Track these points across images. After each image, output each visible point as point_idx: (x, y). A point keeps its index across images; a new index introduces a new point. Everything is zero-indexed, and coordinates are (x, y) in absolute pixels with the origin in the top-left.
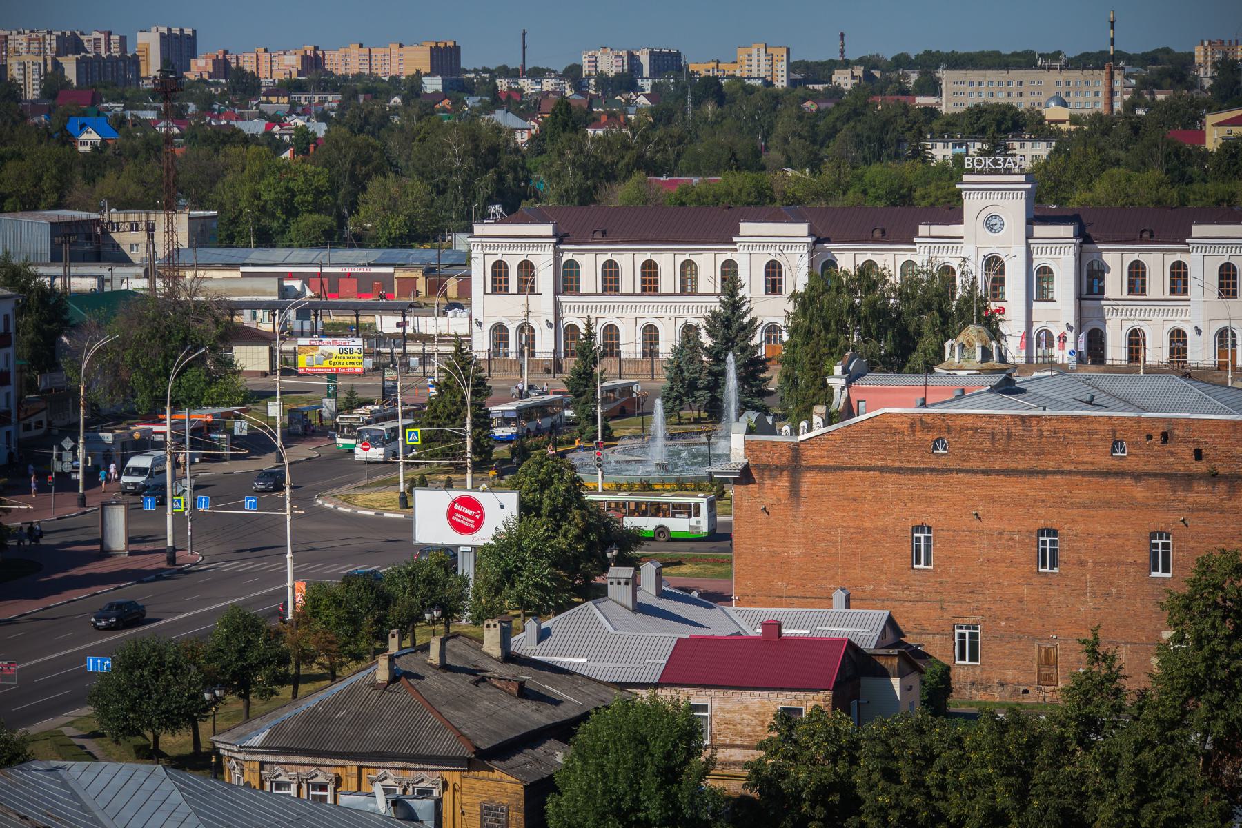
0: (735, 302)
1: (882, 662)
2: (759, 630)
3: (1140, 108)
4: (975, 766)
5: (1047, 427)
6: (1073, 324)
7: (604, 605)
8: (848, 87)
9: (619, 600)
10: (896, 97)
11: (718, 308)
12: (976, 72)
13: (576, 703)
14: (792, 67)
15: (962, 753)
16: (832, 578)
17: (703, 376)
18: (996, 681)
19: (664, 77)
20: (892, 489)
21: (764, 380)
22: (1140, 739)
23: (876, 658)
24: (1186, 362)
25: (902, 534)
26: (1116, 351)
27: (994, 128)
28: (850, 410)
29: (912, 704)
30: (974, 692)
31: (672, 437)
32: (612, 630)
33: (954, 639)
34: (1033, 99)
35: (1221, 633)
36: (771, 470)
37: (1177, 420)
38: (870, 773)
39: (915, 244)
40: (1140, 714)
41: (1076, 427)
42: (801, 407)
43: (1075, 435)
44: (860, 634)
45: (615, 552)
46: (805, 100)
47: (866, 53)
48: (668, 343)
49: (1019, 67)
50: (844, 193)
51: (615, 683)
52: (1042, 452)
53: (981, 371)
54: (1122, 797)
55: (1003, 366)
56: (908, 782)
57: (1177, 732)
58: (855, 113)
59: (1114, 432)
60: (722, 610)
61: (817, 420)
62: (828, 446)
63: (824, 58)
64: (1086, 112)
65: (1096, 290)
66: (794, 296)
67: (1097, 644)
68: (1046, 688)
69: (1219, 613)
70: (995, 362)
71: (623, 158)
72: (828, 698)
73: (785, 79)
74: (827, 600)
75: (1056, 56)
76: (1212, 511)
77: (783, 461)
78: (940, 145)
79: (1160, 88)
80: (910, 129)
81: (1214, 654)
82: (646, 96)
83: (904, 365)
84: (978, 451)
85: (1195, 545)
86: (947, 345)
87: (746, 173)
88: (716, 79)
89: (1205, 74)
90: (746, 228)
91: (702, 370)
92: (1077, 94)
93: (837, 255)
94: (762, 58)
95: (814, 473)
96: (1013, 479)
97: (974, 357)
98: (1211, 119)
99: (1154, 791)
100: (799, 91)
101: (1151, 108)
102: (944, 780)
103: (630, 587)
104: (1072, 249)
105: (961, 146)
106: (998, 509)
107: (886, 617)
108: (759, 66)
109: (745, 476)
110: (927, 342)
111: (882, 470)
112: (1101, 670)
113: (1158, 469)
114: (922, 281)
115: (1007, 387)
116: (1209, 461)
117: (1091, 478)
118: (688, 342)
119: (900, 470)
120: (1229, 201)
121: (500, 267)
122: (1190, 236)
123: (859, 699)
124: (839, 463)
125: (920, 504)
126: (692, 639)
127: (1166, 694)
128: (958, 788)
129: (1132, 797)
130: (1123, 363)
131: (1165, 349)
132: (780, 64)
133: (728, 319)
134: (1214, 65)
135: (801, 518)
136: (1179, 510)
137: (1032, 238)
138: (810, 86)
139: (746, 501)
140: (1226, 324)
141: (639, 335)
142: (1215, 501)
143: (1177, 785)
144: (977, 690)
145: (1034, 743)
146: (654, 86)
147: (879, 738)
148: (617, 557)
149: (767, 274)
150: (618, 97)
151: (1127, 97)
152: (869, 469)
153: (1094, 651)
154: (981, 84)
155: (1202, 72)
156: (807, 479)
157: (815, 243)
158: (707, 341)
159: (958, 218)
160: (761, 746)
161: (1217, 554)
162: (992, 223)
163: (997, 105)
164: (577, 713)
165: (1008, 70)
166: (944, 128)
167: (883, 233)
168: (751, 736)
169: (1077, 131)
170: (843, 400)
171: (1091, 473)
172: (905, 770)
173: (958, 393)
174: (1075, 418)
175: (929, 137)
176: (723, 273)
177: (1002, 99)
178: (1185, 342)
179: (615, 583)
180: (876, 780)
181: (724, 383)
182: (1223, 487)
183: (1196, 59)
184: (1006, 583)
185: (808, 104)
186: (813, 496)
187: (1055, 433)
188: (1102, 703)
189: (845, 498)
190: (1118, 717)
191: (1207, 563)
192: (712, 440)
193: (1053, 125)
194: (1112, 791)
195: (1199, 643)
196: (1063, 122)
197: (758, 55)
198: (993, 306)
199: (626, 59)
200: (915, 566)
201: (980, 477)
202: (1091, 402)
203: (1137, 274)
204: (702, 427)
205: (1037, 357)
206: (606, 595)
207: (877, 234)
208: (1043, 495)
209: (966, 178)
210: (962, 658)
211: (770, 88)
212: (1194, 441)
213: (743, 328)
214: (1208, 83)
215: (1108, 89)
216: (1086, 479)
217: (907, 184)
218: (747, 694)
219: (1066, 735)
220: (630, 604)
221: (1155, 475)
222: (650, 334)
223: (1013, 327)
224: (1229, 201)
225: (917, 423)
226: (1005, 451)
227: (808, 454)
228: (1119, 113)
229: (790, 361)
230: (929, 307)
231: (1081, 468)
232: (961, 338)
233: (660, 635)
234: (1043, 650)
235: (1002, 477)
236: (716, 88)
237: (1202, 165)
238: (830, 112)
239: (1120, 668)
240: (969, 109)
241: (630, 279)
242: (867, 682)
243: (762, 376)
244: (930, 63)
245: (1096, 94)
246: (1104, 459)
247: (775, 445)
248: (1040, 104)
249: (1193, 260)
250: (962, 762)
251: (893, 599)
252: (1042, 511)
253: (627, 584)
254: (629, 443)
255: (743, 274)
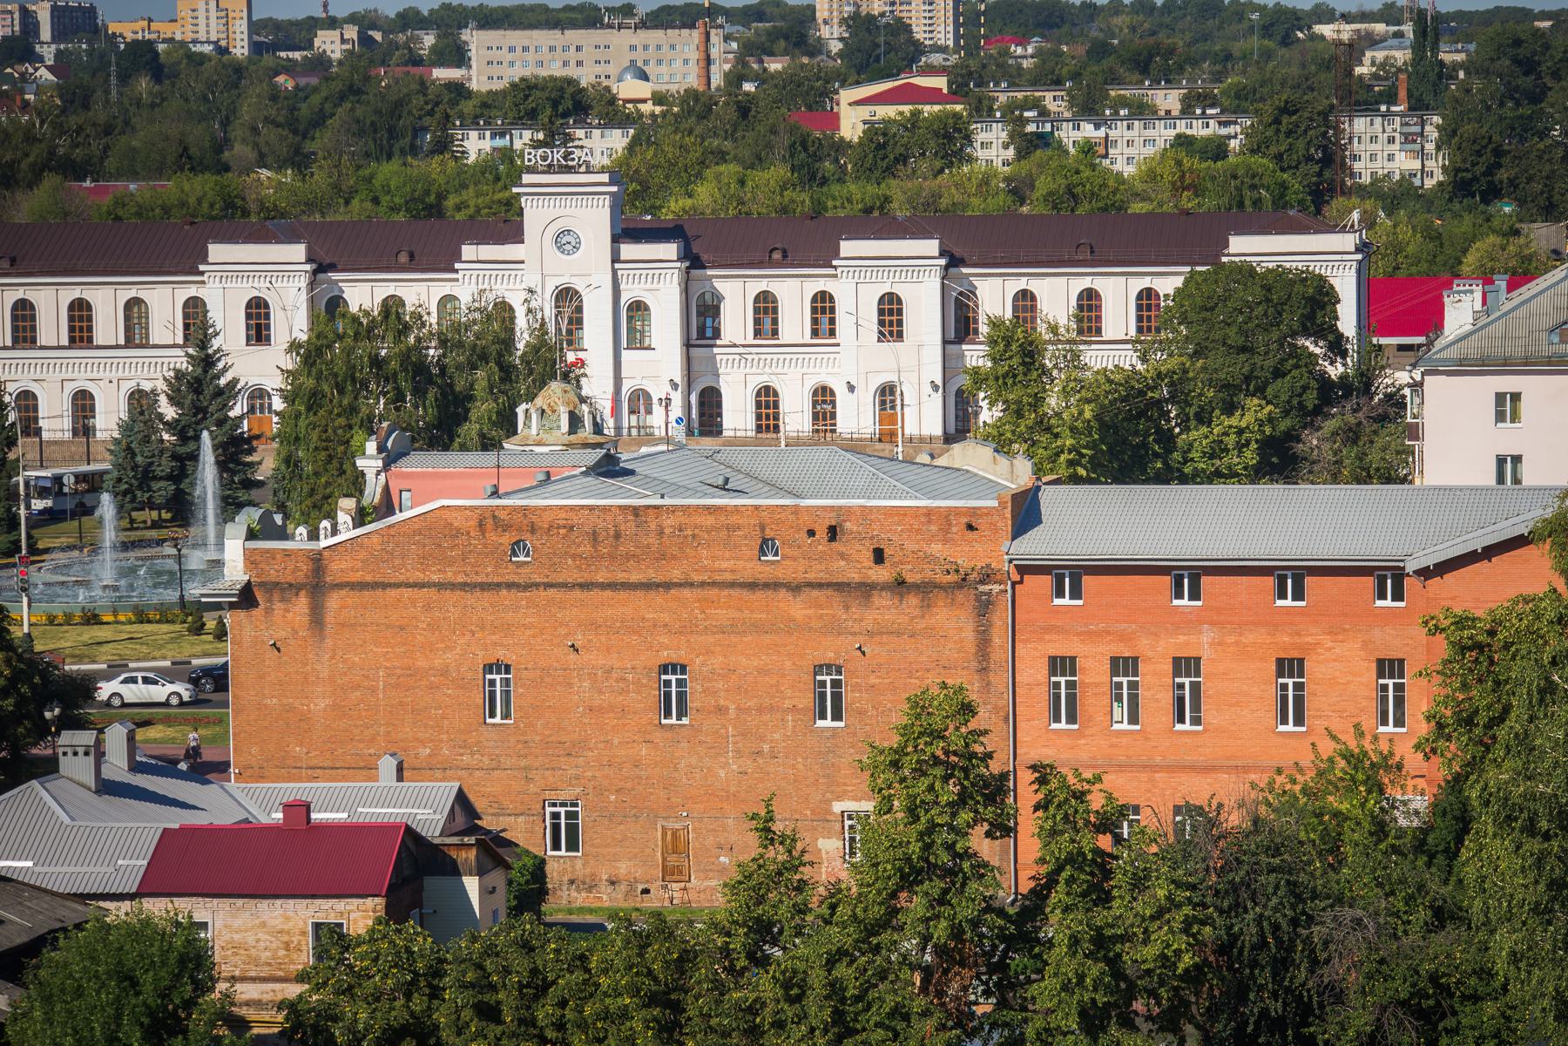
0: (208, 356)
1: (453, 854)
2: (280, 815)
3: (747, 81)
4: (605, 994)
5: (669, 522)
6: (678, 380)
7: (55, 784)
8: (337, 55)
9: (76, 777)
10: (406, 69)
11: (183, 364)
12: (518, 33)
13: (21, 925)
14: (254, 27)
15: (587, 976)
16: (373, 740)
17: (164, 461)
18: (605, 877)
19: (72, 42)
20: (454, 613)
21: (251, 465)
22: (834, 949)
23: (445, 849)
24: (834, 431)
25: (469, 675)
26: (737, 415)
27: (548, 112)
28: (387, 506)
29: (495, 913)
30: (574, 894)
31: (126, 546)
32: (67, 820)
33: (544, 821)
34: (599, 69)
35: (944, 799)
36: (283, 590)
37: (849, 510)
38: (458, 1011)
39: (457, 271)
40: (832, 915)
41: (710, 521)
42: (309, 502)
43: (708, 532)
44: (418, 817)
45: (57, 711)
46: (277, 74)
47: (359, 7)
48: (109, 419)
49: (574, 25)
50: (347, 202)
51: (75, 895)
52: (663, 556)
53: (570, 445)
54: (812, 1030)
55: (599, 439)
56: (512, 1021)
57: (885, 937)
58: (353, 91)
59: (763, 528)
60: (222, 787)
61: (343, 518)
62: (362, 555)
63: (300, 15)
64: (673, 88)
65: (709, 333)
66: (294, 346)
67: (771, 819)
68: (674, 885)
69: (939, 771)
70: (587, 432)
71: (27, 155)
72: (379, 907)
73: (246, 43)
74: (368, 769)
75: (628, 10)
76: (898, 634)
77: (300, 577)
78: (474, 134)
79: (771, 54)
80: (431, 113)
81: (932, 827)
82: (48, 68)
83: (452, 440)
84: (574, 557)
85: (877, 681)
86: (520, 410)
87: (207, 175)
88: (150, 44)
89: (832, 35)
90: (216, 251)
91: (162, 452)
92: (660, 62)
93: (977, 282)
94: (213, 14)
95: (343, 592)
96: (623, 594)
97: (559, 427)
98: (846, 95)
99: (856, 1020)
100: (267, 59)
101: (763, 82)
102: (563, 1016)
103: (92, 758)
104: (676, 276)
105: (502, 135)
106: (603, 639)
107: (455, 791)
108: (208, 25)
109: (246, 598)
110: (482, 409)
111: (440, 586)
112: (778, 854)
113: (823, 577)
114: (475, 322)
115: (609, 467)
116: (894, 565)
117: (732, 592)
118: (142, 413)
119: (464, 586)
120: (882, 208)
121: (891, 302)
122: (837, 255)
123: (421, 907)
124: (379, 578)
125: (494, 633)
126: (183, 829)
127: (869, 885)
128: (582, 1026)
129: (826, 1031)
130: (750, 434)
131: (806, 413)
132: (238, 22)
133: (198, 380)
134: (843, 21)
135: (327, 656)
136: (854, 634)
137: (619, 261)
138: (283, 54)
139: (248, 633)
140: (893, 378)
141: (67, 405)
142: (903, 619)
143: (887, 1010)
144: (578, 890)
145: (686, 960)
146: (59, 55)
147: (471, 959)
148: (59, 717)
149: (248, 316)
150: (9, 70)
151: (727, 67)
152: (422, 585)
153: (768, 830)
154: (525, 49)
155: (825, 32)
156: (333, 601)
157: (315, 272)
158: (169, 412)
159: (514, 234)
160: (301, 978)
161: (935, 691)
162: (565, 241)
163: (553, 79)
164: (22, 939)
165: (563, 29)
166: (478, 111)
167: (412, 256)
168: (270, 964)
169: (664, 114)
170: (379, 490)
171: (733, 585)
172: (506, 999)
173: (542, 477)
174: (708, 508)
175: (458, 123)
176: (186, 316)
177: (556, 70)
178: (833, 403)
179: (70, 754)
180: (467, 1019)
181: (194, 471)
182: (913, 600)
183: (818, 14)
184: (616, 741)
185: (281, 79)
186: (343, 625)
187: (680, 530)
188: (781, 901)
189: (388, 626)
190: (804, 920)
191: (921, 703)
192: (183, 552)
193: (629, 106)
194: (798, 1023)
195: (912, 814)
196: (644, 101)
197: (207, 11)
198: (571, 357)
199: (17, 16)
200: (489, 721)
201: (578, 593)
202: (724, 487)
203: (766, 308)
204: (164, 533)
205: (629, 428)
206: (57, 771)
207: (403, 258)
208: (665, 617)
209: (526, 178)
210: (556, 846)
211: (226, 57)
212: (872, 538)
213: (220, 392)
214: (836, 47)
215: (703, 55)
216: (726, 592)
217: (434, 189)
218: (264, 905)
219: (732, 946)
220: (91, 781)
221: (820, 586)
222: (83, 404)
223: (598, 386)
224: (882, 208)
225: (488, 521)
226: (612, 557)
227: (334, 566)
228: (718, 89)
229: (290, 439)
230: (484, 357)
231: (718, 578)
232: (539, 401)
233: (135, 825)
234: (669, 833)
235: (608, 593)
236: (149, 56)
237: (837, 161)
238: (316, 89)
239: (803, 852)
240: (514, 85)
241: (52, 325)
242: (432, 884)
243: (249, 459)
244: (450, 22)
245: (686, 62)
246: (749, 565)
247: (287, 554)
248: (608, 77)
249: (841, 288)
250: (588, 989)
251: (457, 767)
252: (664, 640)
253: (86, 754)
254: (61, 558)
255: (215, 315)
